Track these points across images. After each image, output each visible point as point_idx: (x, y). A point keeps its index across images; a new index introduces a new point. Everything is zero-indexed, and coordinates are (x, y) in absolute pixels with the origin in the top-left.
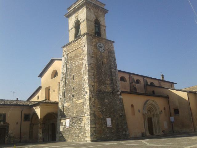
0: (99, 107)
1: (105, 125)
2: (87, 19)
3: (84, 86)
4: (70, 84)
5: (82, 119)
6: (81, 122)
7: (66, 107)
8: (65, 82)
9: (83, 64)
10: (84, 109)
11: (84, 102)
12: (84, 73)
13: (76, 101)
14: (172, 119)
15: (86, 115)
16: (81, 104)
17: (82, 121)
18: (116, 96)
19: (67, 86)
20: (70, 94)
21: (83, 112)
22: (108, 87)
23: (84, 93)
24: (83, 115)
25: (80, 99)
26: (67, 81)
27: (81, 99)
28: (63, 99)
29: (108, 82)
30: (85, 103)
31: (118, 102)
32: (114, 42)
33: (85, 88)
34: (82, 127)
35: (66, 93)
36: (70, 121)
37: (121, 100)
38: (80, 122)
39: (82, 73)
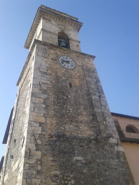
0: (56, 176)
32: (93, 57)
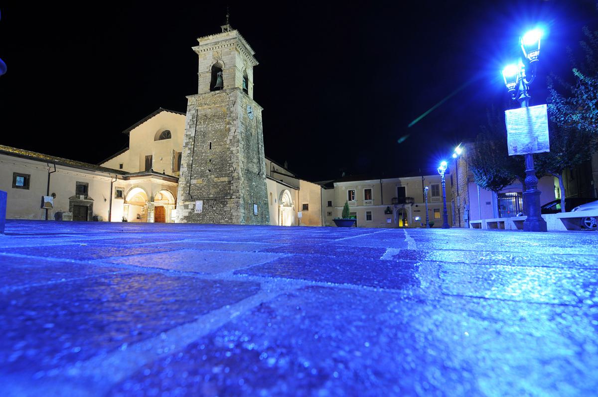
0: (248, 190)
1: (528, 157)
2: (322, 187)
3: (230, 160)
4: (204, 154)
5: (227, 202)
6: (225, 205)
7: (195, 185)
8: (192, 149)
9: (229, 130)
10: (230, 189)
11: (230, 181)
12: (230, 142)
13: (215, 179)
14: (300, 214)
15: (233, 197)
16: (224, 183)
17: (227, 204)
18: (262, 179)
19: (196, 156)
20: (203, 168)
21: (229, 193)
22: (255, 167)
23: (231, 169)
24: (229, 197)
25: (223, 177)
26: (195, 149)
27: (225, 177)
28: (189, 173)
29: (255, 160)
30: (232, 182)
31: (263, 187)
33: (232, 163)
34: (225, 211)
35: (193, 166)
36: (204, 204)
37: (265, 184)
38: (222, 206)
39: (228, 142)
